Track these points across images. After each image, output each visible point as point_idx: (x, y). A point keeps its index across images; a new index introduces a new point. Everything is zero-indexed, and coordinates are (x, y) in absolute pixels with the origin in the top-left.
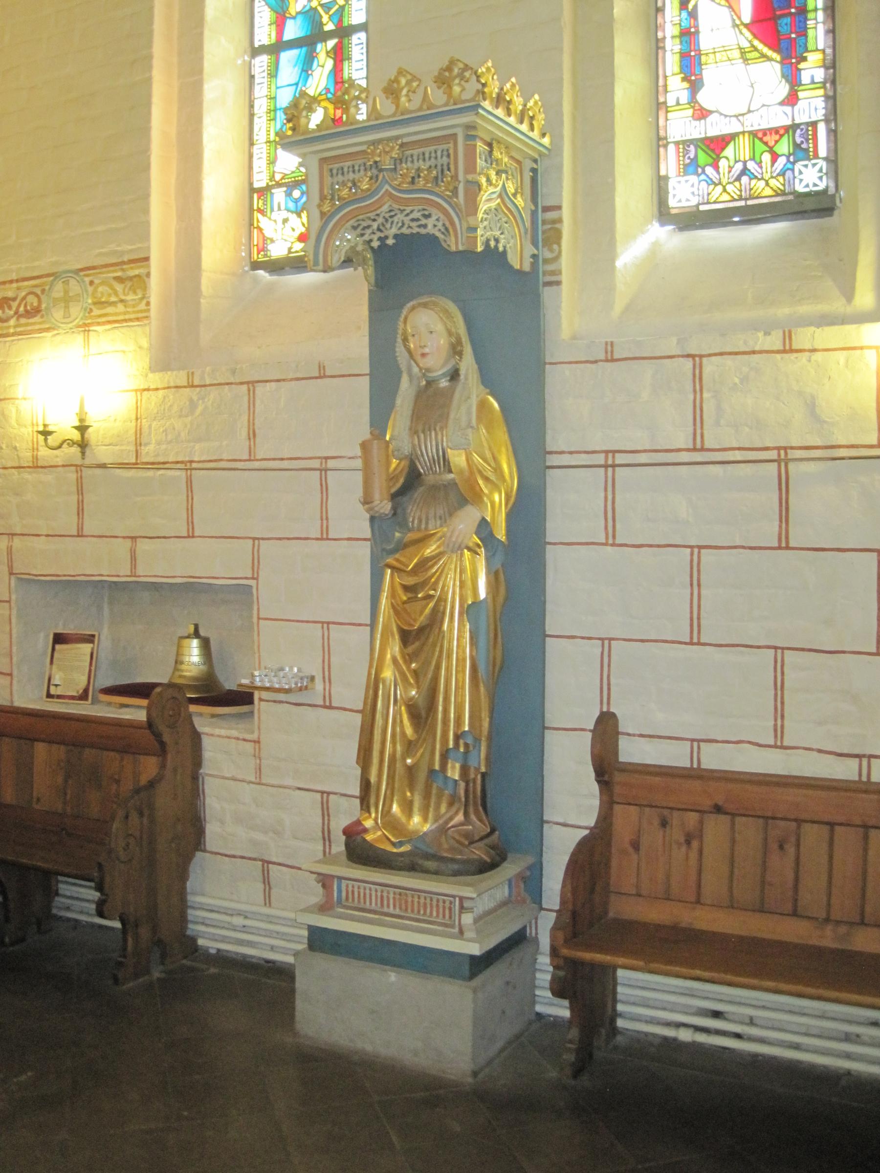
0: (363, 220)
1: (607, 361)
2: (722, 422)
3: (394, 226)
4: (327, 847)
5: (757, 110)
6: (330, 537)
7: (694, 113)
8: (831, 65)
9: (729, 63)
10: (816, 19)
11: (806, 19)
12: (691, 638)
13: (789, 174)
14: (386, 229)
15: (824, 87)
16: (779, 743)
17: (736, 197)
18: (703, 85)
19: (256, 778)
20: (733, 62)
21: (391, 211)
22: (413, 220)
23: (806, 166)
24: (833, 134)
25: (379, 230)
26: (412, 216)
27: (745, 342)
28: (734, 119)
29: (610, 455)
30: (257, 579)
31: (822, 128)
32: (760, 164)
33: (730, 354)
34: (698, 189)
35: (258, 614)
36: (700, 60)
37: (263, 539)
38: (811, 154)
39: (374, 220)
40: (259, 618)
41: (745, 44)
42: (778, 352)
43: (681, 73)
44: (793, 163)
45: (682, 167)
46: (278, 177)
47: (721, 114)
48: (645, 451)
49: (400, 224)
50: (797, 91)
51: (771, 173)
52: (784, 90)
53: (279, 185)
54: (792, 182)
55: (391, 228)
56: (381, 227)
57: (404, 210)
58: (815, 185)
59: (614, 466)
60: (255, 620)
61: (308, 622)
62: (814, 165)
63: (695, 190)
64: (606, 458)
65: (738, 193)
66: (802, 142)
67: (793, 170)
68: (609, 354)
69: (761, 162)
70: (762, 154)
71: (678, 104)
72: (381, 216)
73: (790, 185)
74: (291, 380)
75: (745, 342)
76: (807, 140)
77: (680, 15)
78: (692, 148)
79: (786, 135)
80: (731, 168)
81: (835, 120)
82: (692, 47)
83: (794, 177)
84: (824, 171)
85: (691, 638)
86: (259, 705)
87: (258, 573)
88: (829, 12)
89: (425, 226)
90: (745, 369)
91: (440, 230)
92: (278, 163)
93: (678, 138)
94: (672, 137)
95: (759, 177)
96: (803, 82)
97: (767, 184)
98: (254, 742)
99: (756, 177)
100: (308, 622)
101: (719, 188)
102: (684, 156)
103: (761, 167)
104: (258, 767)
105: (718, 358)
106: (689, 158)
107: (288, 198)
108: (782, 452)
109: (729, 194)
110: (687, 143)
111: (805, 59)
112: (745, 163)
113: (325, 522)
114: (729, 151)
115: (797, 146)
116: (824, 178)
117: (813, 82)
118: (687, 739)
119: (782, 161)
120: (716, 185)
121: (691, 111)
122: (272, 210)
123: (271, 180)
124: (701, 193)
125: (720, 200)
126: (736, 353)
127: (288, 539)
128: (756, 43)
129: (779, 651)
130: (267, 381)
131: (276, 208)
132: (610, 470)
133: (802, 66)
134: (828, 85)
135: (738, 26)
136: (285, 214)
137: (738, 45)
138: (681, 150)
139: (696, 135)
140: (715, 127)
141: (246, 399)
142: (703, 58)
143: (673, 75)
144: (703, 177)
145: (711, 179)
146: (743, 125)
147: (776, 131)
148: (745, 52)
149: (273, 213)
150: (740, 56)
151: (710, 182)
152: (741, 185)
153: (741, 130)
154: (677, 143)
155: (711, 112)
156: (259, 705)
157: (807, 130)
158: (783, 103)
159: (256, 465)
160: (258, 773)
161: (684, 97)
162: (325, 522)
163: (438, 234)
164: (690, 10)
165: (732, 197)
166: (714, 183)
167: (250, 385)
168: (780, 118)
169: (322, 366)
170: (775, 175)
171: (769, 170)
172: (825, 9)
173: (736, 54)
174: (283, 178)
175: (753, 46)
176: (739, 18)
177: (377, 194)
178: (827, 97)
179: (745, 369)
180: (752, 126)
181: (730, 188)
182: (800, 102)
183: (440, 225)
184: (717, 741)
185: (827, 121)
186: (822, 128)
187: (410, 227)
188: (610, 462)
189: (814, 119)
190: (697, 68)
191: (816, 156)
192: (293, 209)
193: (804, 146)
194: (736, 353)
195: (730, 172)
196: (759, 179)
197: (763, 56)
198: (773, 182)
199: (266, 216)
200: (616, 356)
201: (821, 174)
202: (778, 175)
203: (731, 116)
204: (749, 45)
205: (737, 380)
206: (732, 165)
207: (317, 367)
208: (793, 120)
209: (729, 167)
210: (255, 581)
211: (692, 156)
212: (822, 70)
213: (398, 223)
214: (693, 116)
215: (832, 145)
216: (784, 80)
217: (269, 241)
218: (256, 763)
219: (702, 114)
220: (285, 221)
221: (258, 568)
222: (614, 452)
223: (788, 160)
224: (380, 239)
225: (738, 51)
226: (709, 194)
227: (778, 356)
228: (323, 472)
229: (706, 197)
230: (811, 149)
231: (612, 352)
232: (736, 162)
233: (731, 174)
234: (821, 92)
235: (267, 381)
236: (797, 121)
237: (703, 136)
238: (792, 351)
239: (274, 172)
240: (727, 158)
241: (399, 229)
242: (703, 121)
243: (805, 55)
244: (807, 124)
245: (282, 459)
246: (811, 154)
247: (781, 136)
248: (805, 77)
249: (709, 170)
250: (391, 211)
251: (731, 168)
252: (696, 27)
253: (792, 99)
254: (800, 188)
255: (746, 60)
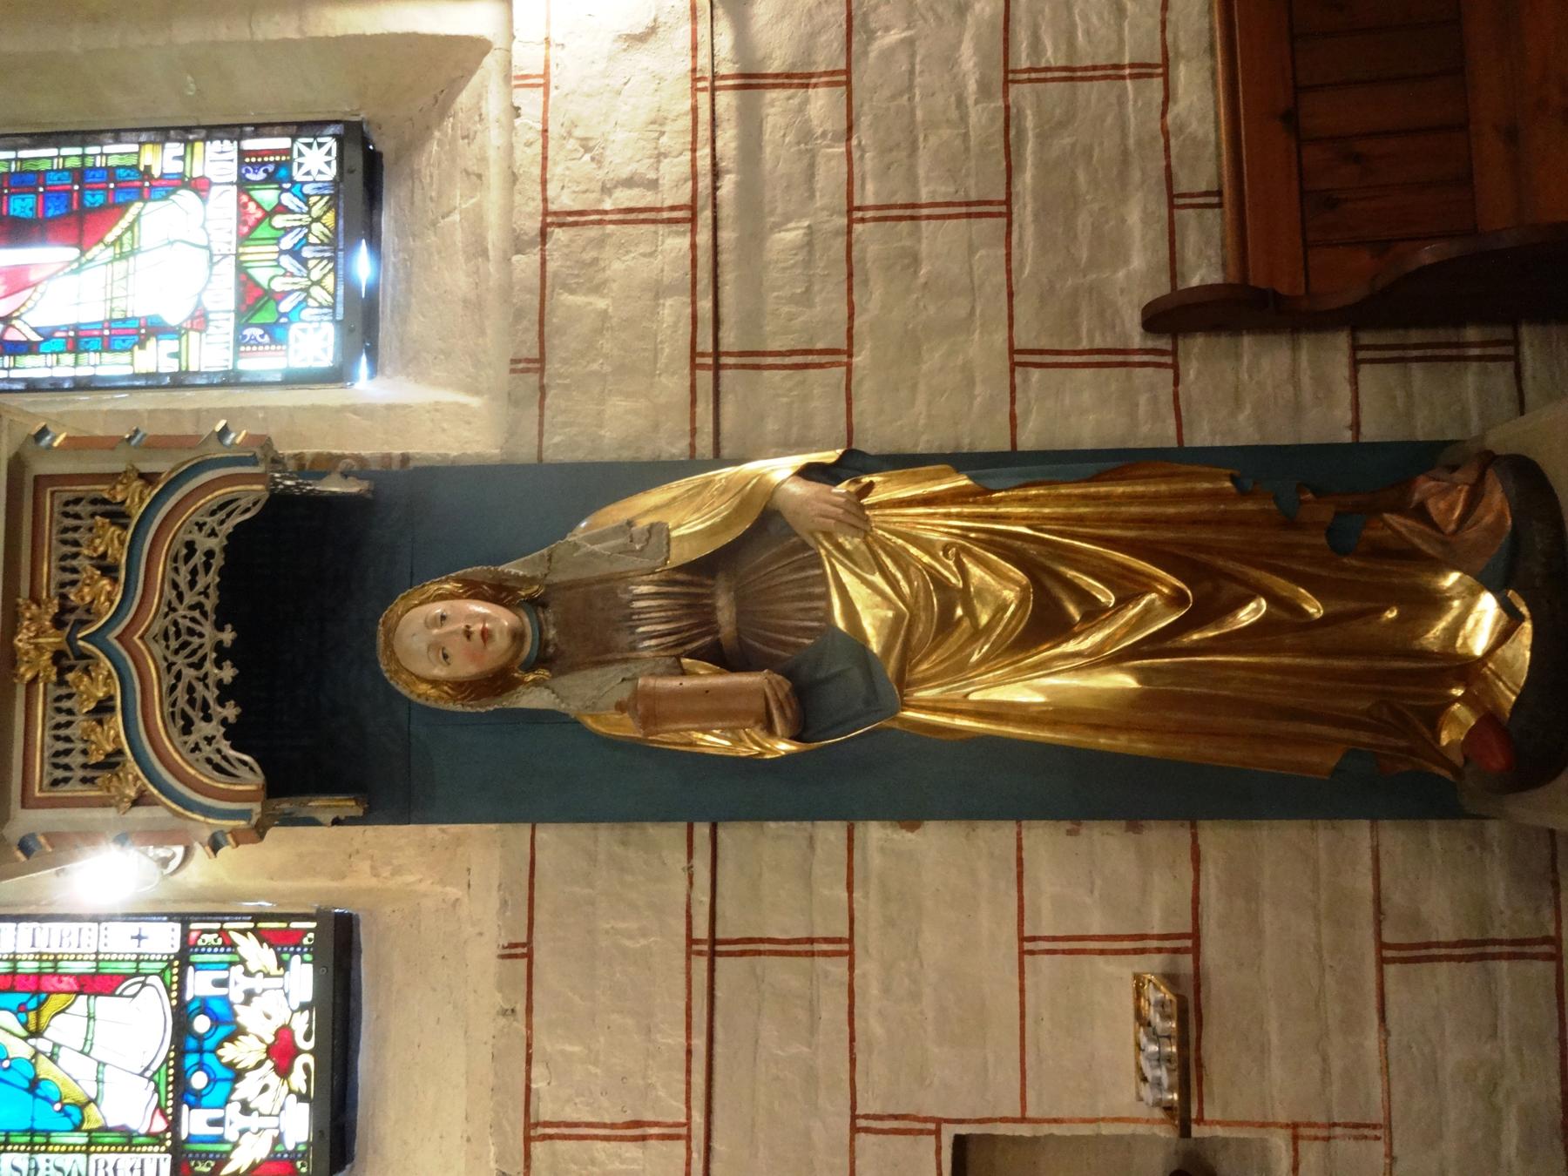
0: (174, 704)
1: (542, 370)
2: (652, 175)
3: (198, 628)
4: (1496, 949)
5: (208, 235)
6: (846, 935)
7: (196, 330)
8: (163, 134)
9: (131, 277)
10: (94, 156)
11: (94, 168)
12: (999, 215)
13: (307, 189)
14: (201, 646)
15: (193, 142)
16: (1160, 70)
17: (331, 266)
18: (157, 317)
19: (1377, 1138)
20: (131, 271)
21: (166, 637)
22: (192, 584)
23: (300, 165)
24: (260, 129)
25: (198, 666)
26: (184, 586)
27: (529, 144)
28: (216, 269)
29: (699, 360)
30: (939, 1121)
31: (249, 144)
32: (287, 230)
33: (544, 168)
34: (311, 322)
35: (1014, 1120)
36: (118, 320)
37: (853, 1107)
38: (284, 158)
39: (178, 676)
40: (1023, 1120)
41: (110, 252)
42: (546, 94)
43: (131, 350)
44: (294, 183)
45: (273, 347)
46: (160, 1125)
47: (204, 289)
48: (694, 303)
49: (196, 614)
50: (191, 178)
51: (302, 213)
52: (186, 197)
53: (174, 1125)
54: (320, 185)
55: (201, 635)
56: (195, 659)
57: (169, 603)
58: (329, 153)
59: (717, 354)
60: (1024, 1130)
61: (1022, 991)
62: (300, 154)
63: (310, 327)
64: (703, 367)
65: (325, 262)
66: (266, 171)
67: (303, 183)
68: (531, 365)
69: (284, 228)
70: (273, 228)
71: (177, 355)
72: (171, 658)
73: (325, 188)
74: (529, 1026)
75: (529, 144)
76: (264, 164)
77: (46, 354)
78: (248, 332)
79: (252, 193)
80: (287, 274)
81: (241, 126)
82: (96, 333)
83: (315, 182)
84: (310, 140)
85: (999, 215)
86: (1213, 1123)
87: (926, 1120)
88: (89, 138)
89: (210, 554)
90: (572, 144)
91: (222, 522)
92: (133, 1126)
93: (230, 354)
94: (226, 363)
95: (306, 231)
96: (181, 170)
97: (318, 219)
98: (1296, 1139)
99: (306, 236)
100: (1022, 991)
101: (315, 291)
102: (259, 344)
103: (293, 228)
104: (1354, 1132)
105: (549, 186)
106: (262, 336)
107: (205, 1101)
108: (700, 85)
109: (325, 275)
110: (239, 341)
111: (148, 168)
112: (282, 252)
113: (818, 947)
114: (261, 276)
115: (271, 179)
116: (320, 140)
117: (182, 158)
118: (1171, 216)
119: (288, 200)
120: (309, 296)
121: (193, 335)
122: (220, 1139)
123: (161, 1142)
124: (318, 318)
125: (331, 289)
126: (545, 158)
127: (852, 1039)
128: (110, 237)
129: (1003, 209)
130: (528, 1089)
131: (217, 1131)
132: (724, 360)
133: (156, 173)
134: (191, 137)
135: (81, 265)
136: (234, 1109)
137: (106, 264)
138: (248, 348)
139: (230, 326)
140: (223, 297)
141: (560, 1145)
142: (116, 315)
143: (132, 364)
144: (293, 316)
145: (300, 303)
146: (225, 256)
147: (242, 207)
148: (121, 253)
149: (227, 1137)
150: (124, 262)
151: (304, 305)
152: (314, 258)
153: (233, 258)
154: (237, 354)
155: (199, 302)
156: (1213, 1123)
157: (250, 164)
158: (204, 200)
159: (698, 1118)
160: (1366, 1132)
161: (168, 345)
162: (818, 947)
163: (229, 527)
164: (40, 339)
165: (330, 271)
166: (305, 300)
167: (533, 1133)
168: (225, 200)
169: (507, 951)
170: (306, 209)
171: (298, 216)
172: (83, 144)
173: (120, 266)
174: (164, 1115)
175: (113, 244)
176: (70, 263)
177: (124, 659)
178: (209, 138)
179: (572, 144)
180: (229, 243)
181: (315, 275)
182: (207, 175)
183: (211, 522)
184: (1168, 167)
185: (239, 139)
186: (249, 144)
187: (205, 593)
188: (709, 361)
189: (234, 155)
190: (130, 324)
191: (288, 152)
192: (226, 1086)
193: (271, 168)
194: (545, 158)
195: (292, 275)
196: (310, 231)
197: (130, 228)
198: (316, 212)
199: (228, 1153)
200: (535, 354)
201: (315, 145)
202: (307, 204)
203: (211, 274)
204: (111, 249)
205: (587, 157)
206: (282, 272)
207: (508, 961)
208: (231, 183)
209: (284, 275)
210: (944, 1126)
211: (258, 332)
212: (168, 145)
213: (193, 620)
214: (200, 332)
215: (277, 130)
216: (172, 197)
217: (279, 1148)
218: (1344, 1137)
219: (200, 320)
220: (246, 1109)
221: (916, 1119)
222: (694, 353)
223: (288, 190)
224: (218, 664)
225: (116, 263)
226: (321, 306)
227: (553, 93)
228: (719, 948)
229: (326, 310)
230: (278, 158)
231: (528, 361)
232: (279, 266)
233: (296, 272)
234: (199, 146)
235: (528, 1089)
236: (235, 179)
237: (232, 316)
238: (546, 75)
239: (148, 1135)
240: (271, 279)
241: (204, 614)
242: (211, 316)
243: (142, 168)
244: (241, 163)
245: (689, 1052)
246: (284, 158)
247: (251, 199)
248: (175, 167)
249: (285, 306)
250: (166, 637)
251: (287, 274)
252: (68, 328)
253: (200, 186)
254: (331, 173)
255: (133, 252)
